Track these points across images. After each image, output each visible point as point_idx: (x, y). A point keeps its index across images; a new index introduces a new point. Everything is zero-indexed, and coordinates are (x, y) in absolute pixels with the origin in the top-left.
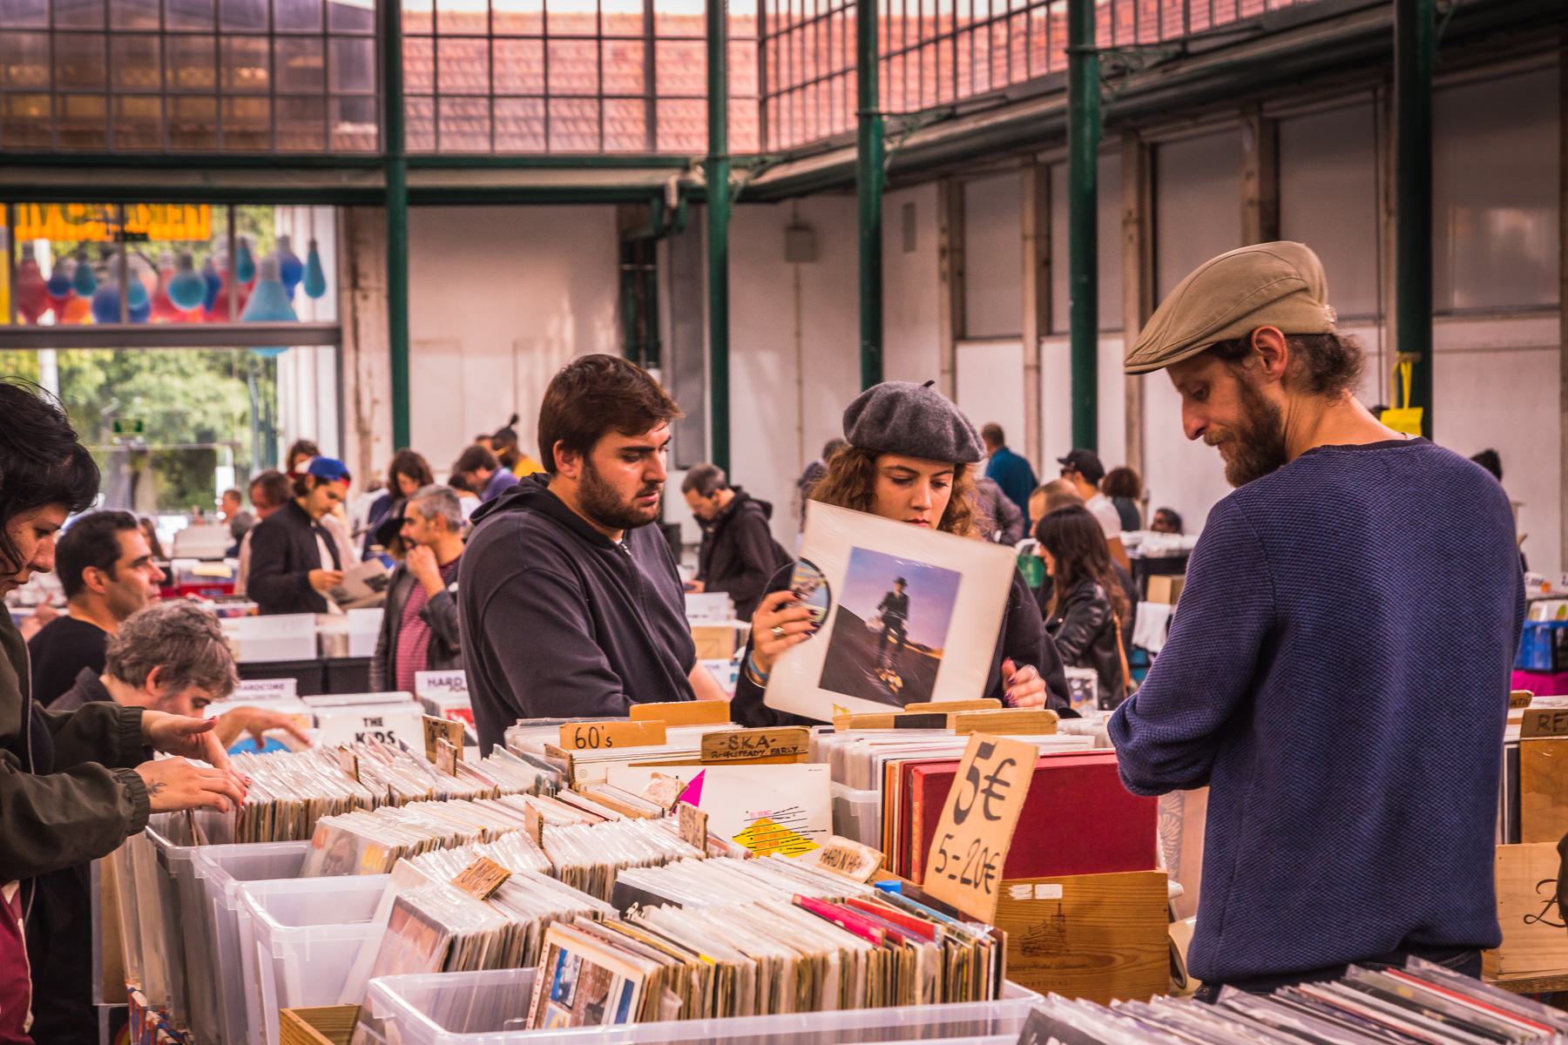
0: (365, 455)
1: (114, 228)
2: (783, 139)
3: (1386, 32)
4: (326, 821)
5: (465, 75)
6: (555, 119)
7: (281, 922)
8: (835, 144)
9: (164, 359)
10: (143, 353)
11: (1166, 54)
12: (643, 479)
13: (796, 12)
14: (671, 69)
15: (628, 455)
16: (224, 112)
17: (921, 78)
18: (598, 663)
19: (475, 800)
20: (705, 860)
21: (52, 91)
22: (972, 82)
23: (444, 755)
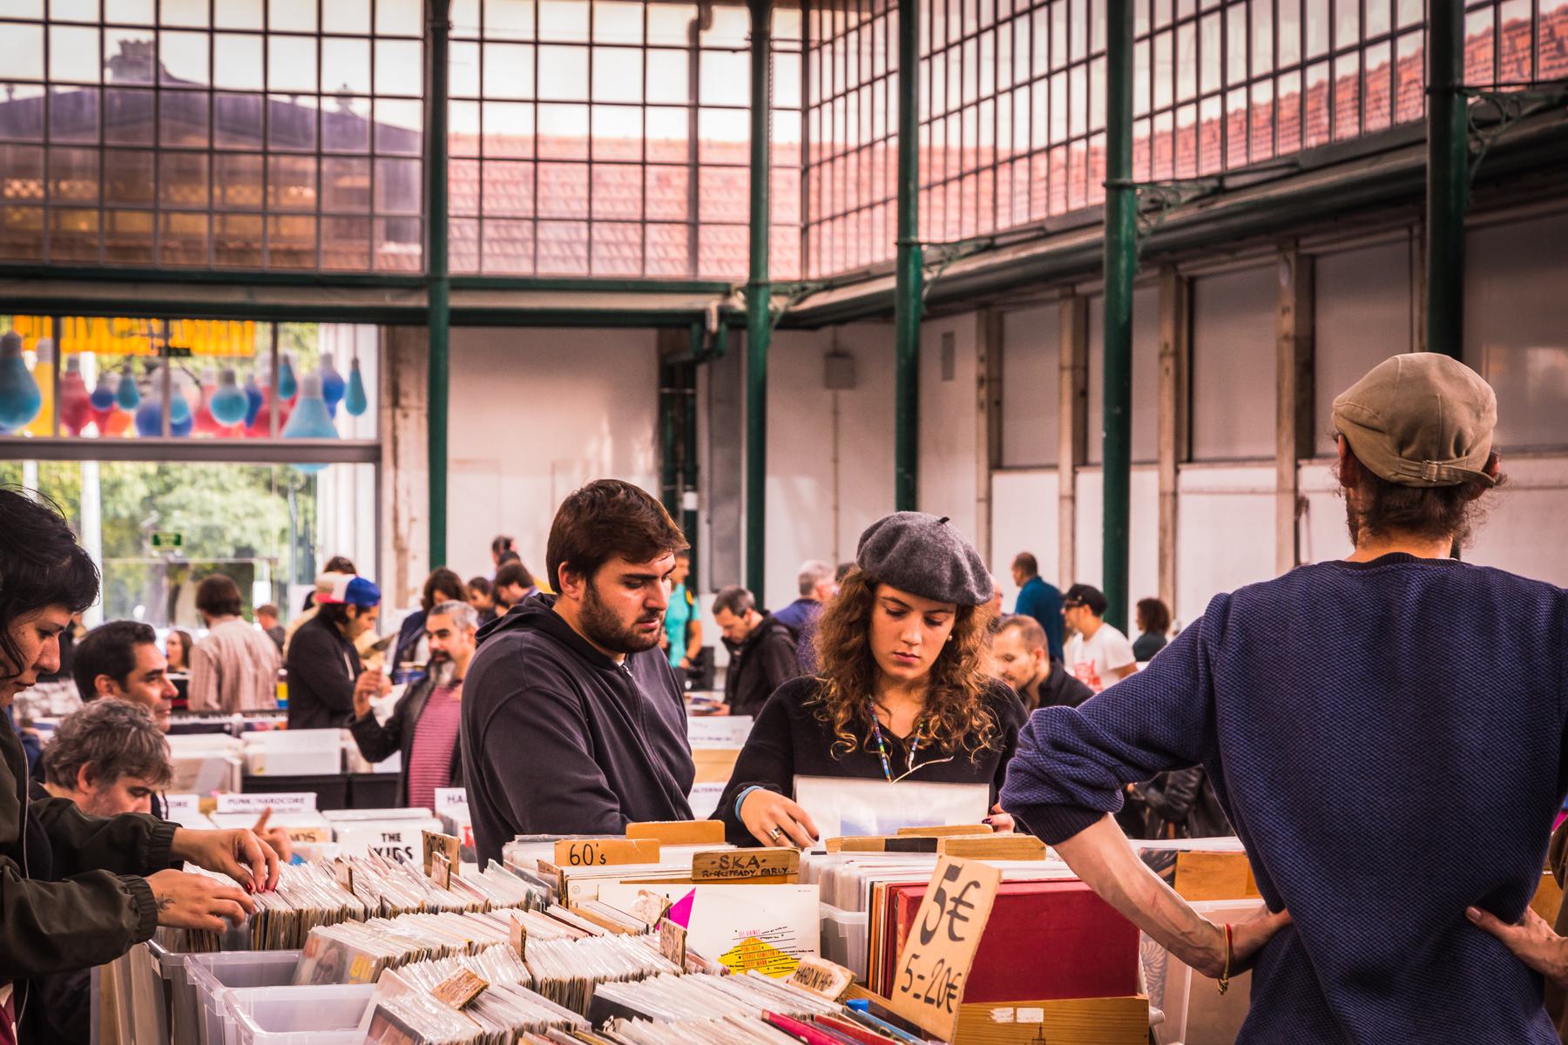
0: (402, 572)
1: (160, 342)
2: (824, 267)
3: (1419, 171)
4: (318, 930)
5: (510, 197)
6: (598, 243)
7: (268, 1029)
8: (875, 272)
9: (205, 474)
10: (185, 467)
11: (1202, 189)
12: (644, 605)
13: (839, 140)
14: (715, 196)
15: (630, 582)
16: (271, 230)
19: (466, 913)
20: (682, 976)
21: (100, 206)
22: (1011, 214)
23: (439, 870)
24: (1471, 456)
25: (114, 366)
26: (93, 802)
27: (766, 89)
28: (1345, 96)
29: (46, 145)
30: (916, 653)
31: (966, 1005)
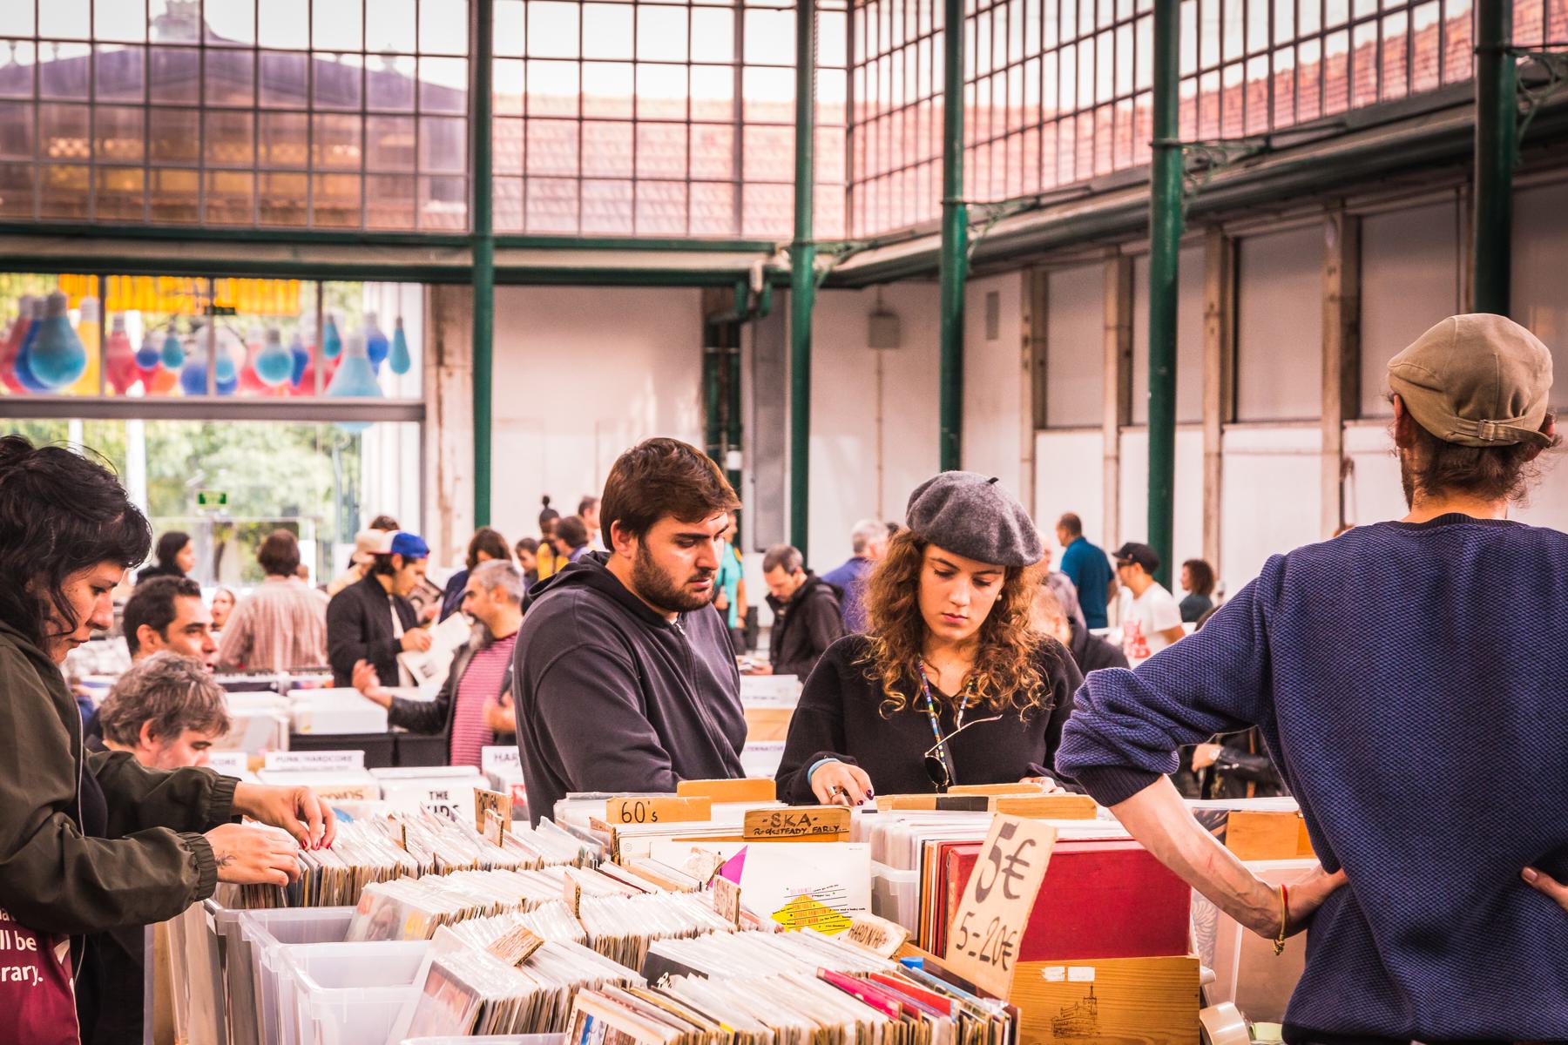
0: (446, 530)
1: (206, 301)
2: (872, 224)
3: (1467, 131)
5: (555, 156)
7: (323, 985)
8: (920, 231)
9: (250, 433)
10: (230, 426)
12: (696, 565)
15: (683, 541)
16: (316, 189)
17: (1006, 167)
18: (649, 739)
19: (519, 870)
20: (736, 933)
22: (1057, 173)
23: (491, 827)
24: (1527, 416)
25: (160, 325)
26: (157, 759)
27: (810, 47)
28: (1393, 56)
29: (92, 104)
30: (964, 614)
31: (1024, 964)
